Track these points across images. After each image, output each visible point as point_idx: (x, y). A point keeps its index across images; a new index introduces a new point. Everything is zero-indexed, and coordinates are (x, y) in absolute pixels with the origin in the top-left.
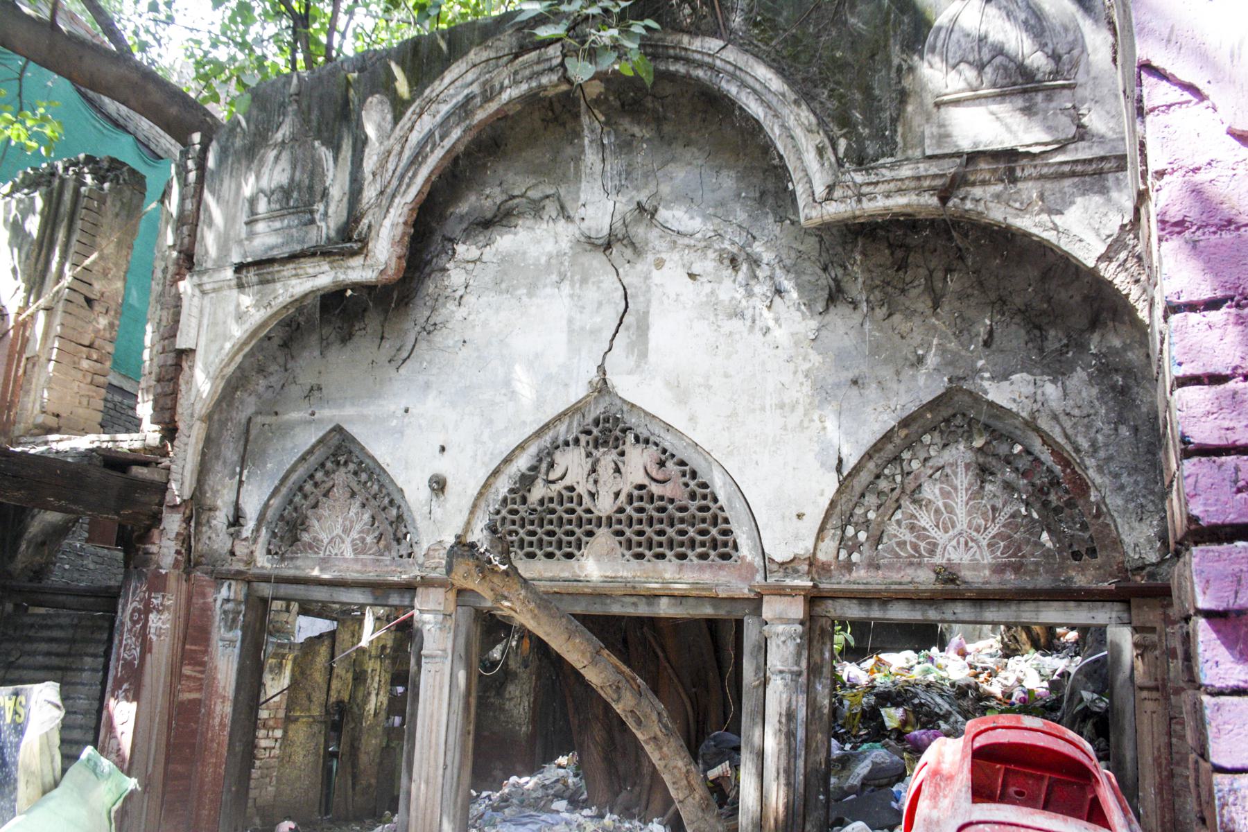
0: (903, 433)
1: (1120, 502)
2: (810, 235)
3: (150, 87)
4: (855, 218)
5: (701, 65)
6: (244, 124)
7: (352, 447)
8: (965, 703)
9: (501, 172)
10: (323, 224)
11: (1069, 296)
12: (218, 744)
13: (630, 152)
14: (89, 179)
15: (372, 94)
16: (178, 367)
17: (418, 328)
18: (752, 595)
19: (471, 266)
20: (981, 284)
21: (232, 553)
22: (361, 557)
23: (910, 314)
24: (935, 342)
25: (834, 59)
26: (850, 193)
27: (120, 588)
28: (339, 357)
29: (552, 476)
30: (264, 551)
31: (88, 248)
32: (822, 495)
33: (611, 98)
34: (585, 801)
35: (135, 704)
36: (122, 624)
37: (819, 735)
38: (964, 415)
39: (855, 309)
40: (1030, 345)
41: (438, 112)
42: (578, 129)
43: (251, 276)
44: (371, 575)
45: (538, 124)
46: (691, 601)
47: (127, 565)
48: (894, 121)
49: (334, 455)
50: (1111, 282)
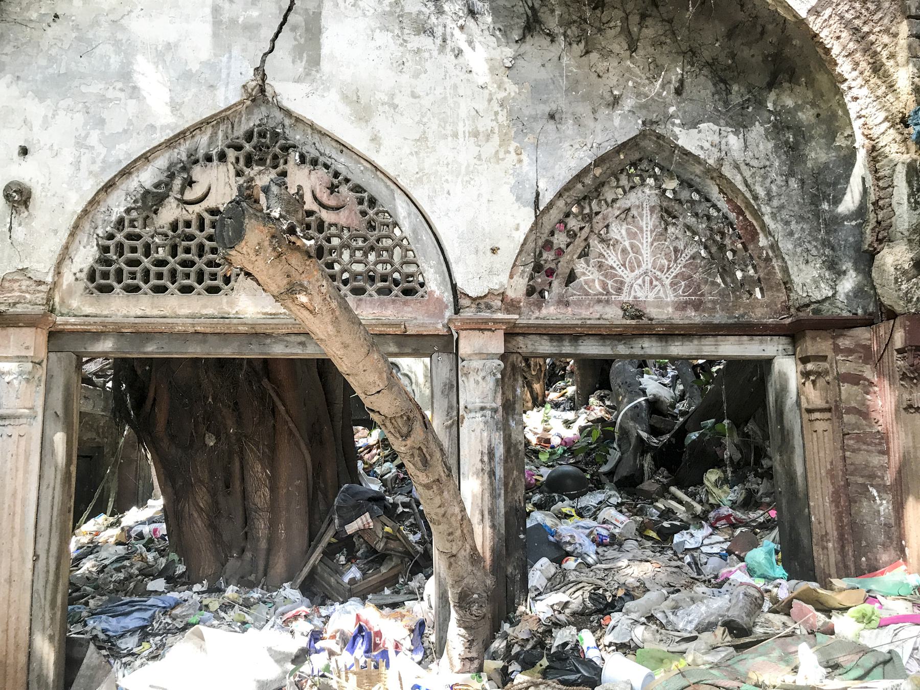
1: (790, 246)
23: (606, 54)
29: (189, 195)
32: (517, 229)
40: (717, 97)
50: (816, 35)
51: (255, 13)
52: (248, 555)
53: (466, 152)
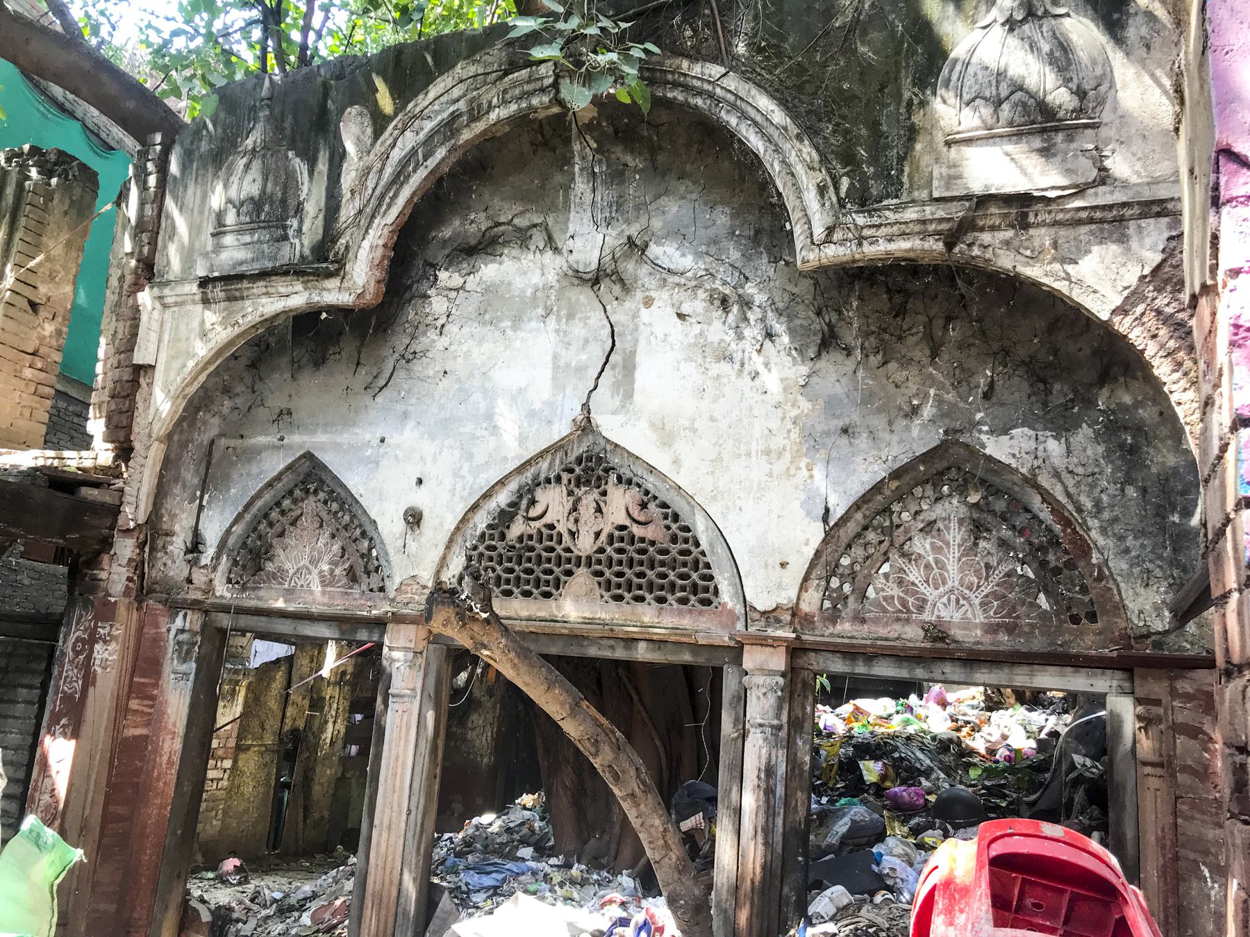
0: (894, 485)
1: (1124, 566)
2: (805, 277)
3: (104, 77)
4: (854, 261)
5: (700, 93)
6: (210, 126)
7: (323, 476)
8: (947, 759)
9: (487, 197)
10: (297, 241)
11: (1080, 349)
12: (165, 783)
13: (622, 182)
14: (34, 173)
15: (351, 104)
16: (135, 384)
17: (396, 356)
18: (732, 644)
19: (453, 294)
20: (983, 333)
21: (189, 581)
22: (329, 589)
23: (906, 362)
24: (932, 392)
25: (840, 90)
26: (850, 235)
27: (62, 615)
28: (310, 382)
29: (532, 513)
30: (224, 580)
31: (37, 247)
32: (807, 544)
33: (604, 124)
34: (551, 848)
35: (73, 742)
36: (63, 654)
37: (799, 794)
38: (959, 469)
39: (848, 355)
41: (422, 129)
42: (568, 155)
43: (218, 292)
44: (339, 606)
45: (527, 148)
46: (669, 646)
47: (71, 591)
48: (901, 160)
49: (303, 483)
50: (1125, 336)
51: (584, 357)
52: (606, 837)
53: (758, 469)
